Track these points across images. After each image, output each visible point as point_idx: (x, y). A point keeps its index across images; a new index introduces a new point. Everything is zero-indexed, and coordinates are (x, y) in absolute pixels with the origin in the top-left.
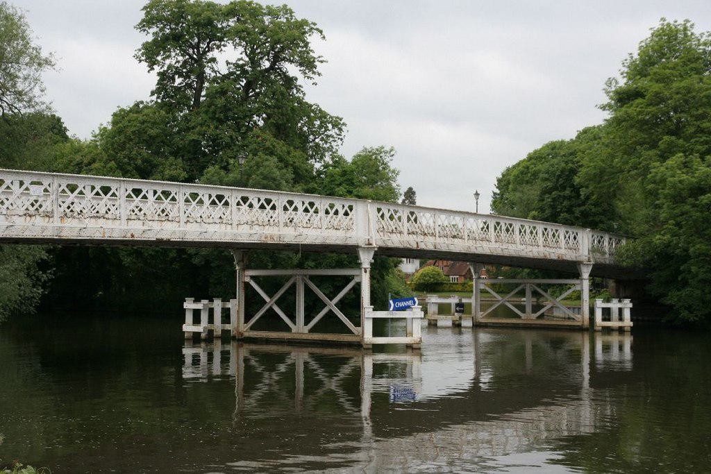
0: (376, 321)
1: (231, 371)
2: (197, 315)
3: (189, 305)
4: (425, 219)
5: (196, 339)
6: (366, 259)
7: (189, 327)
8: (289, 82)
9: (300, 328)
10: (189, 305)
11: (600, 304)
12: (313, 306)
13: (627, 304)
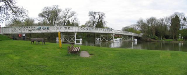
0: (77, 41)
1: (100, 43)
2: (97, 39)
3: (96, 38)
4: (112, 30)
5: (97, 41)
6: (76, 34)
7: (96, 40)
8: (170, 27)
9: (107, 41)
10: (96, 38)
11: (134, 39)
12: (70, 39)
13: (137, 39)
